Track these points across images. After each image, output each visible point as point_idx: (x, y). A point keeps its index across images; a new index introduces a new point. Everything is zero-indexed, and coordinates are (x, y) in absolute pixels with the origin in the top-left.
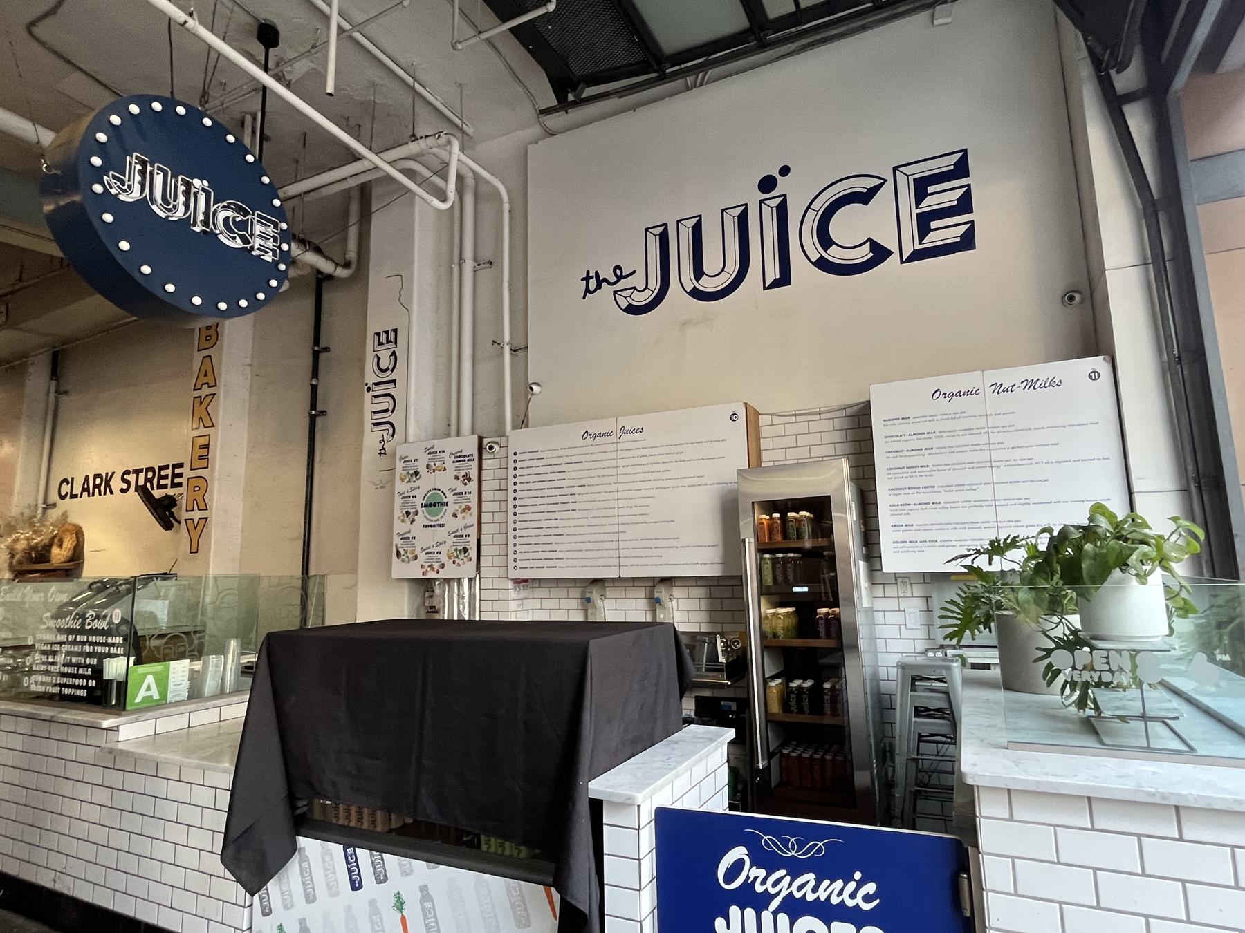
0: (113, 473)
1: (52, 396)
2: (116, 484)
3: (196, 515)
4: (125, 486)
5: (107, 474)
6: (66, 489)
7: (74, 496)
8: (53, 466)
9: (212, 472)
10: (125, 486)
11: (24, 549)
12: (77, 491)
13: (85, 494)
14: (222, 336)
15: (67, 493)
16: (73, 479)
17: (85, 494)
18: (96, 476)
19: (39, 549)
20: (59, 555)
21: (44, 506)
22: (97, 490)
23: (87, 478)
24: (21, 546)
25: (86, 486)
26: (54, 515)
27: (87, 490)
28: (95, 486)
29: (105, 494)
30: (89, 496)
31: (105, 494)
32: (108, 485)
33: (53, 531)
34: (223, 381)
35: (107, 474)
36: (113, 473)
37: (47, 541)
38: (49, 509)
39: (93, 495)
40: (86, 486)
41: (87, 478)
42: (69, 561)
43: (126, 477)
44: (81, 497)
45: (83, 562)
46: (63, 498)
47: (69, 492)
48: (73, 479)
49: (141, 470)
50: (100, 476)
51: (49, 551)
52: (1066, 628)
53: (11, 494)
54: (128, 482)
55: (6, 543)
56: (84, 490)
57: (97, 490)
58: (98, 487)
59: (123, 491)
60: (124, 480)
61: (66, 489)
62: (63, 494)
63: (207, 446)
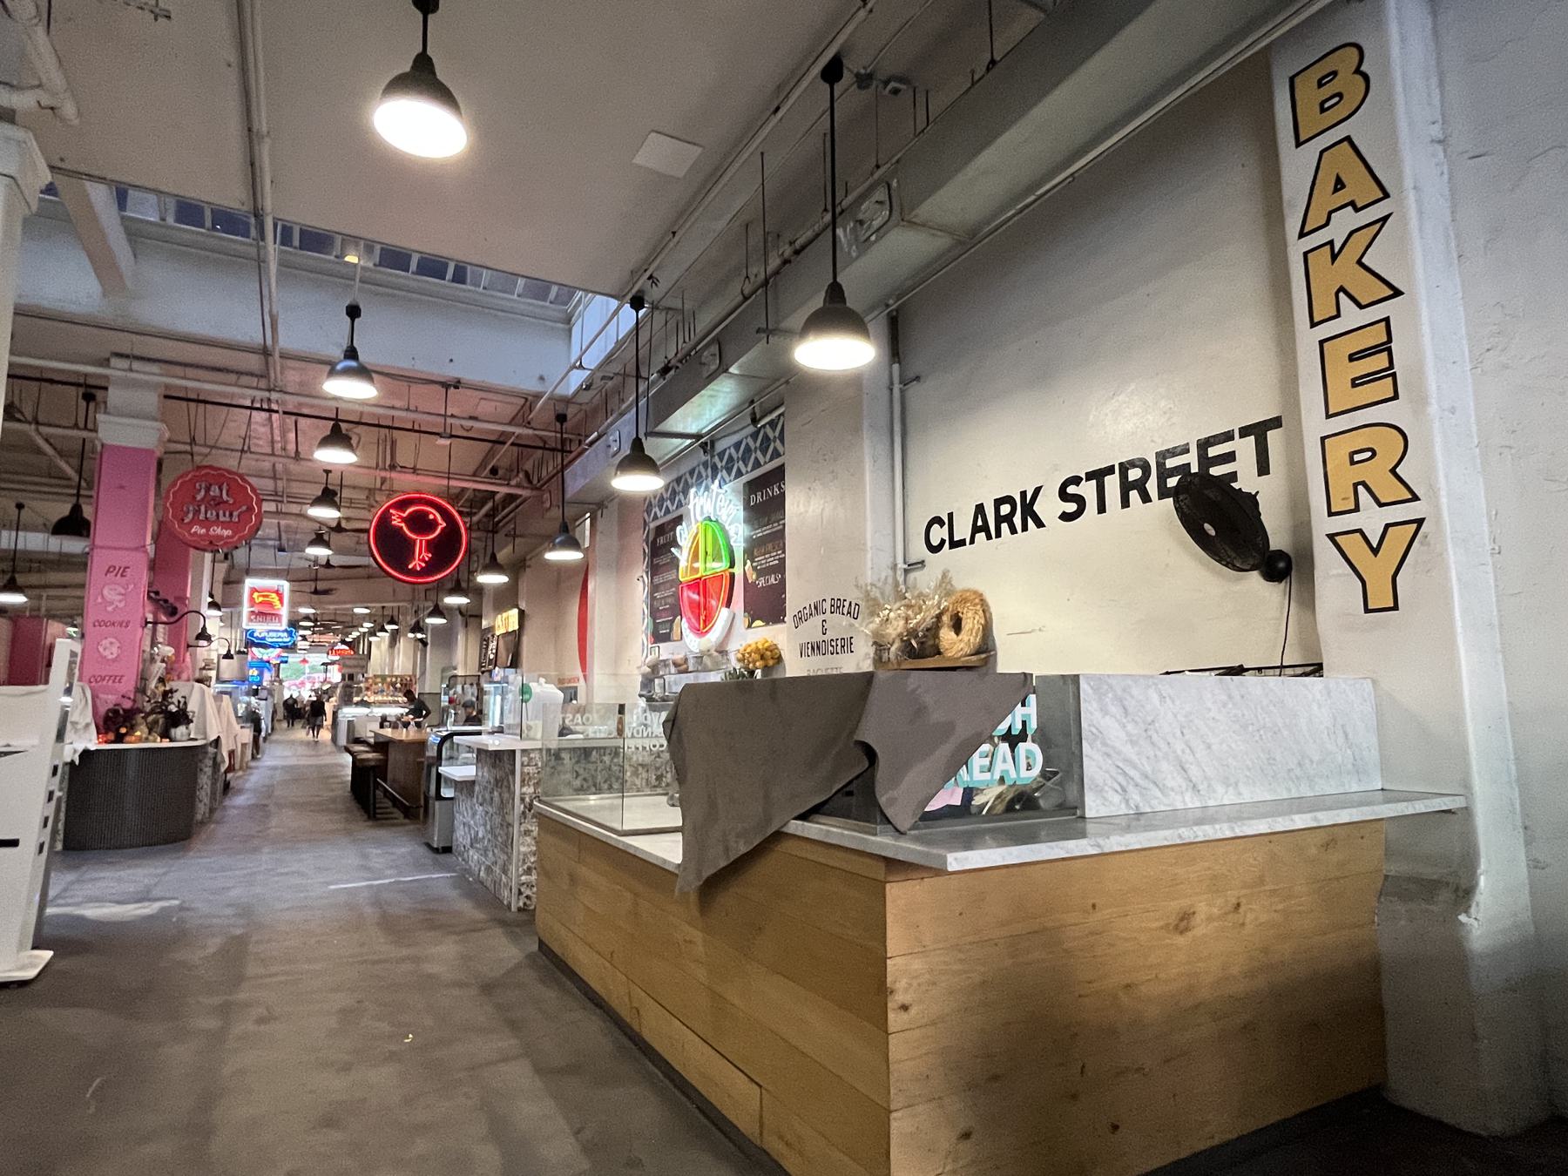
0: (1037, 491)
1: (897, 388)
2: (1049, 506)
3: (1372, 520)
4: (1071, 507)
5: (1024, 494)
6: (938, 534)
7: (955, 544)
8: (908, 502)
9: (1421, 401)
10: (1071, 507)
11: (900, 635)
12: (963, 530)
13: (981, 536)
14: (433, 374)
15: (943, 541)
16: (951, 516)
17: (981, 536)
18: (998, 503)
19: (920, 634)
20: (955, 645)
21: (906, 566)
22: (1004, 526)
23: (980, 509)
24: (895, 629)
25: (980, 523)
26: (926, 580)
27: (985, 528)
28: (999, 519)
29: (1025, 528)
30: (989, 537)
31: (1025, 528)
32: (1029, 511)
33: (939, 603)
34: (1408, 183)
35: (1024, 494)
36: (1037, 491)
37: (929, 621)
38: (913, 570)
39: (998, 535)
40: (980, 523)
41: (980, 509)
42: (977, 653)
43: (1071, 490)
44: (972, 542)
45: (996, 654)
46: (935, 549)
47: (947, 538)
48: (951, 516)
49: (1110, 470)
50: (1008, 500)
51: (936, 636)
52: (22, 418)
53: (865, 550)
54: (1080, 501)
55: (872, 626)
56: (976, 530)
57: (1004, 526)
58: (1008, 519)
59: (1066, 517)
60: (1064, 495)
61: (938, 534)
62: (935, 542)
63: (1385, 348)
